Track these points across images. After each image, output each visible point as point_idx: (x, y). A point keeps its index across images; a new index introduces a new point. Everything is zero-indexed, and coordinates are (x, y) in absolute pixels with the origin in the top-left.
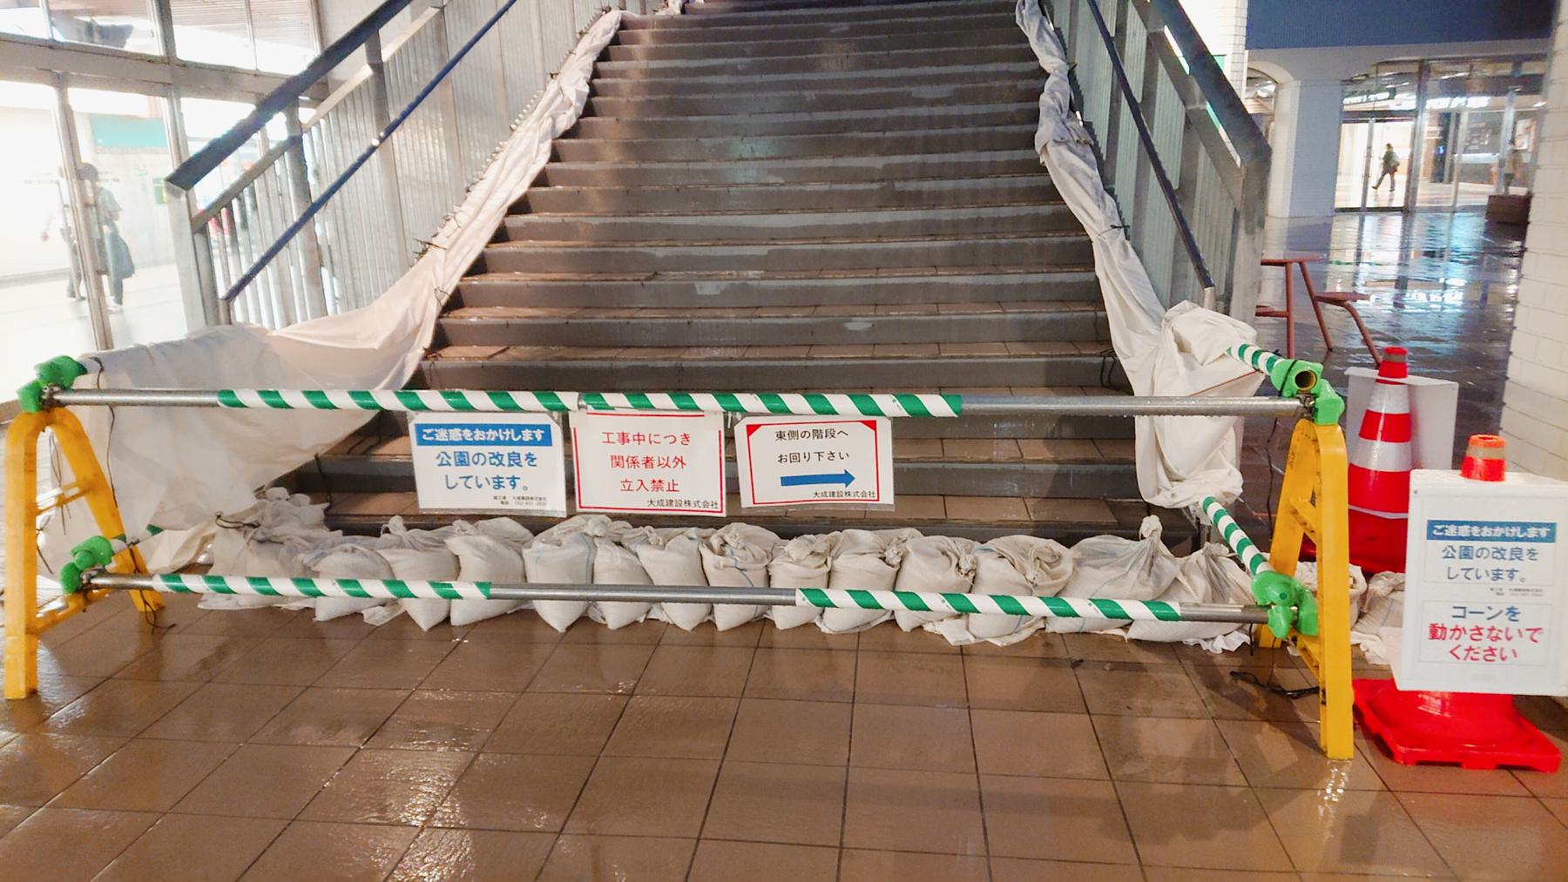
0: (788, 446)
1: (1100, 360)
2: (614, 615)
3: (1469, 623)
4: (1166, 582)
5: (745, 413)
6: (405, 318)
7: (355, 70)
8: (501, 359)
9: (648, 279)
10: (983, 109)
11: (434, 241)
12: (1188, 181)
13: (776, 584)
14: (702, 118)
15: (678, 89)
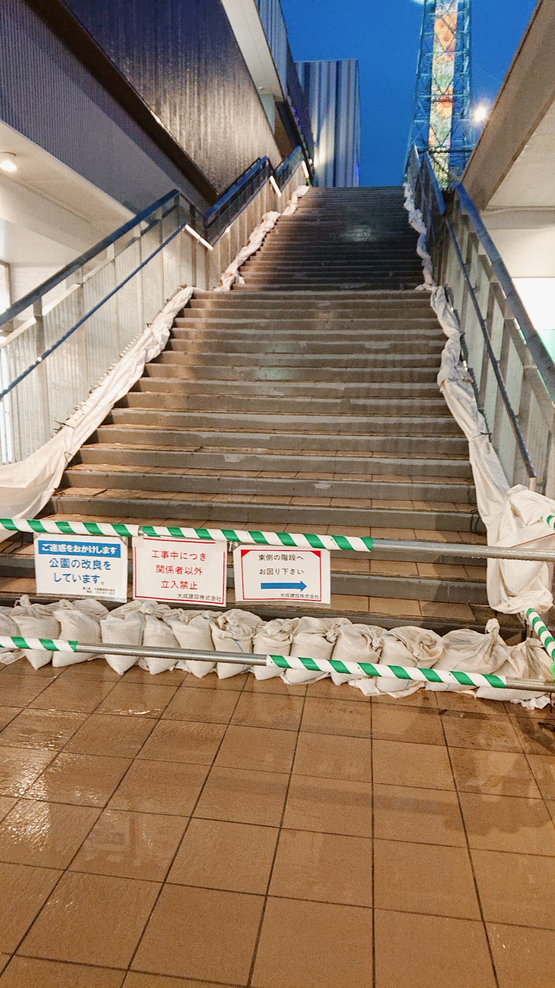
0: (266, 564)
1: (470, 516)
2: (154, 666)
4: (500, 662)
5: (240, 543)
6: (45, 468)
7: (27, 317)
9: (195, 451)
10: (407, 357)
11: (67, 423)
12: (524, 412)
13: (257, 651)
14: (237, 355)
15: (225, 336)
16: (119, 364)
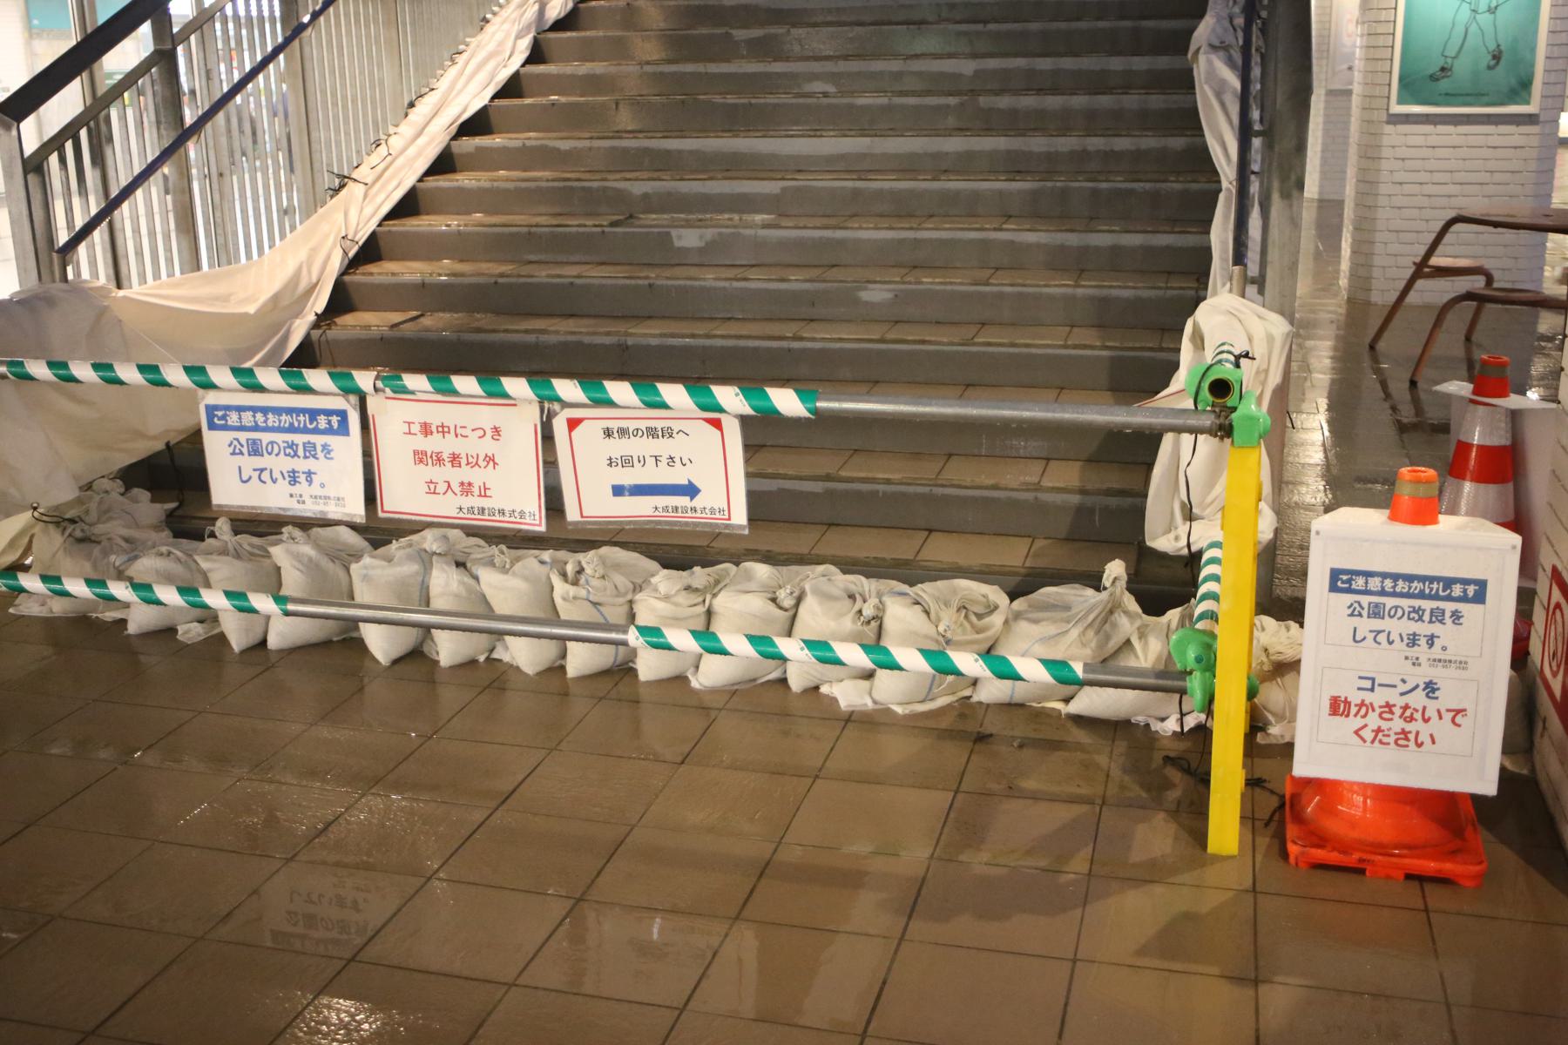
0: (618, 447)
3: (1378, 698)
5: (565, 405)
8: (409, 330)
16: (480, 37)
